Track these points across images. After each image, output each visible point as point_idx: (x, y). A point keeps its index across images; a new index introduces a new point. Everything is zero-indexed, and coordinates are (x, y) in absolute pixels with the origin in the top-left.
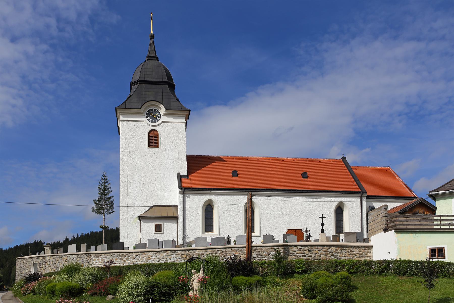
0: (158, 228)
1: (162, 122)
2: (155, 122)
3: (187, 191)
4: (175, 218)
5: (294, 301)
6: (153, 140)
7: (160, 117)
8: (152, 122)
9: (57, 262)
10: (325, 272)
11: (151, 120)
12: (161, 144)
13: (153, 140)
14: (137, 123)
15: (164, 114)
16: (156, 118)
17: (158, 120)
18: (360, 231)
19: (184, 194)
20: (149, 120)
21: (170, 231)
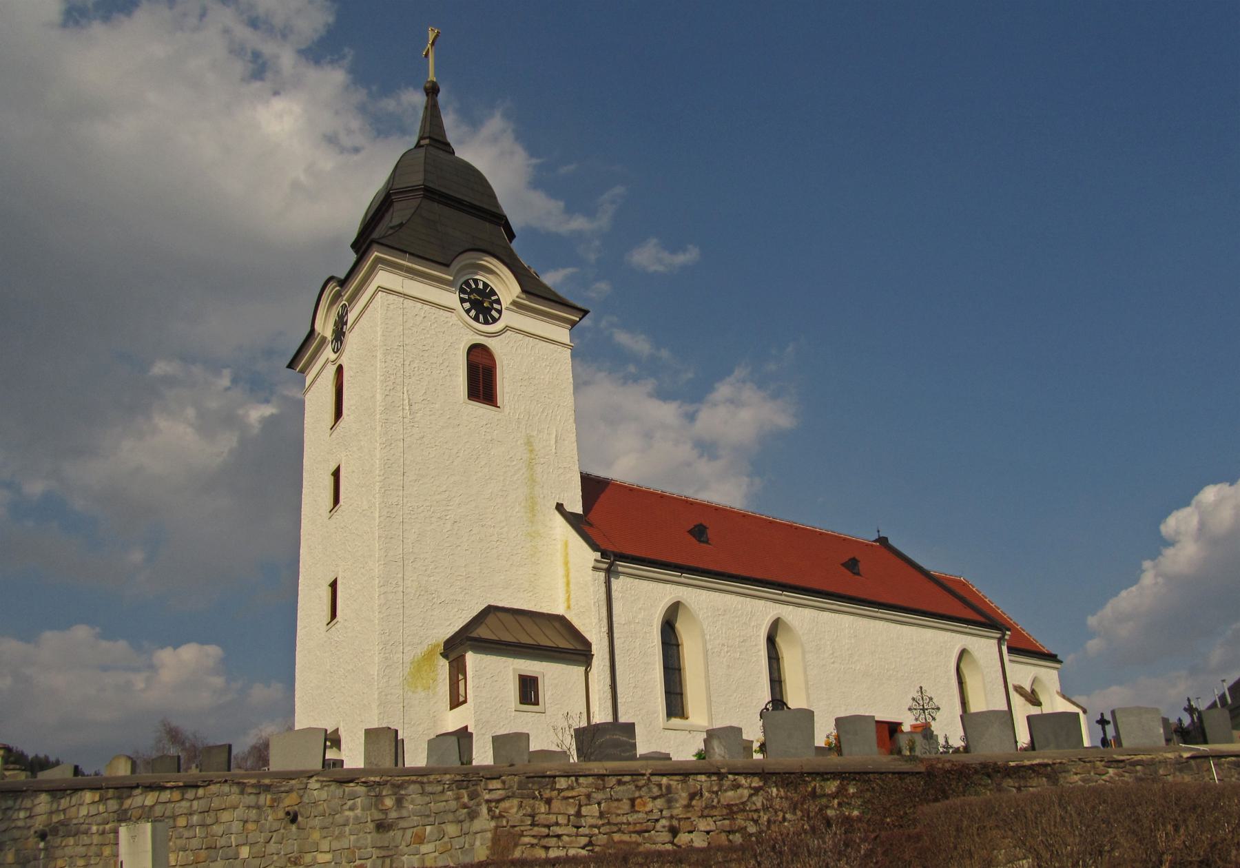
0: (528, 690)
1: (507, 328)
2: (486, 322)
3: (622, 566)
4: (580, 653)
5: (1076, 864)
6: (482, 380)
7: (500, 312)
8: (476, 319)
9: (225, 816)
10: (917, 830)
11: (473, 313)
12: (506, 397)
13: (482, 380)
14: (434, 310)
15: (514, 303)
16: (489, 310)
17: (495, 320)
18: (1006, 708)
19: (610, 573)
20: (468, 312)
21: (571, 698)
